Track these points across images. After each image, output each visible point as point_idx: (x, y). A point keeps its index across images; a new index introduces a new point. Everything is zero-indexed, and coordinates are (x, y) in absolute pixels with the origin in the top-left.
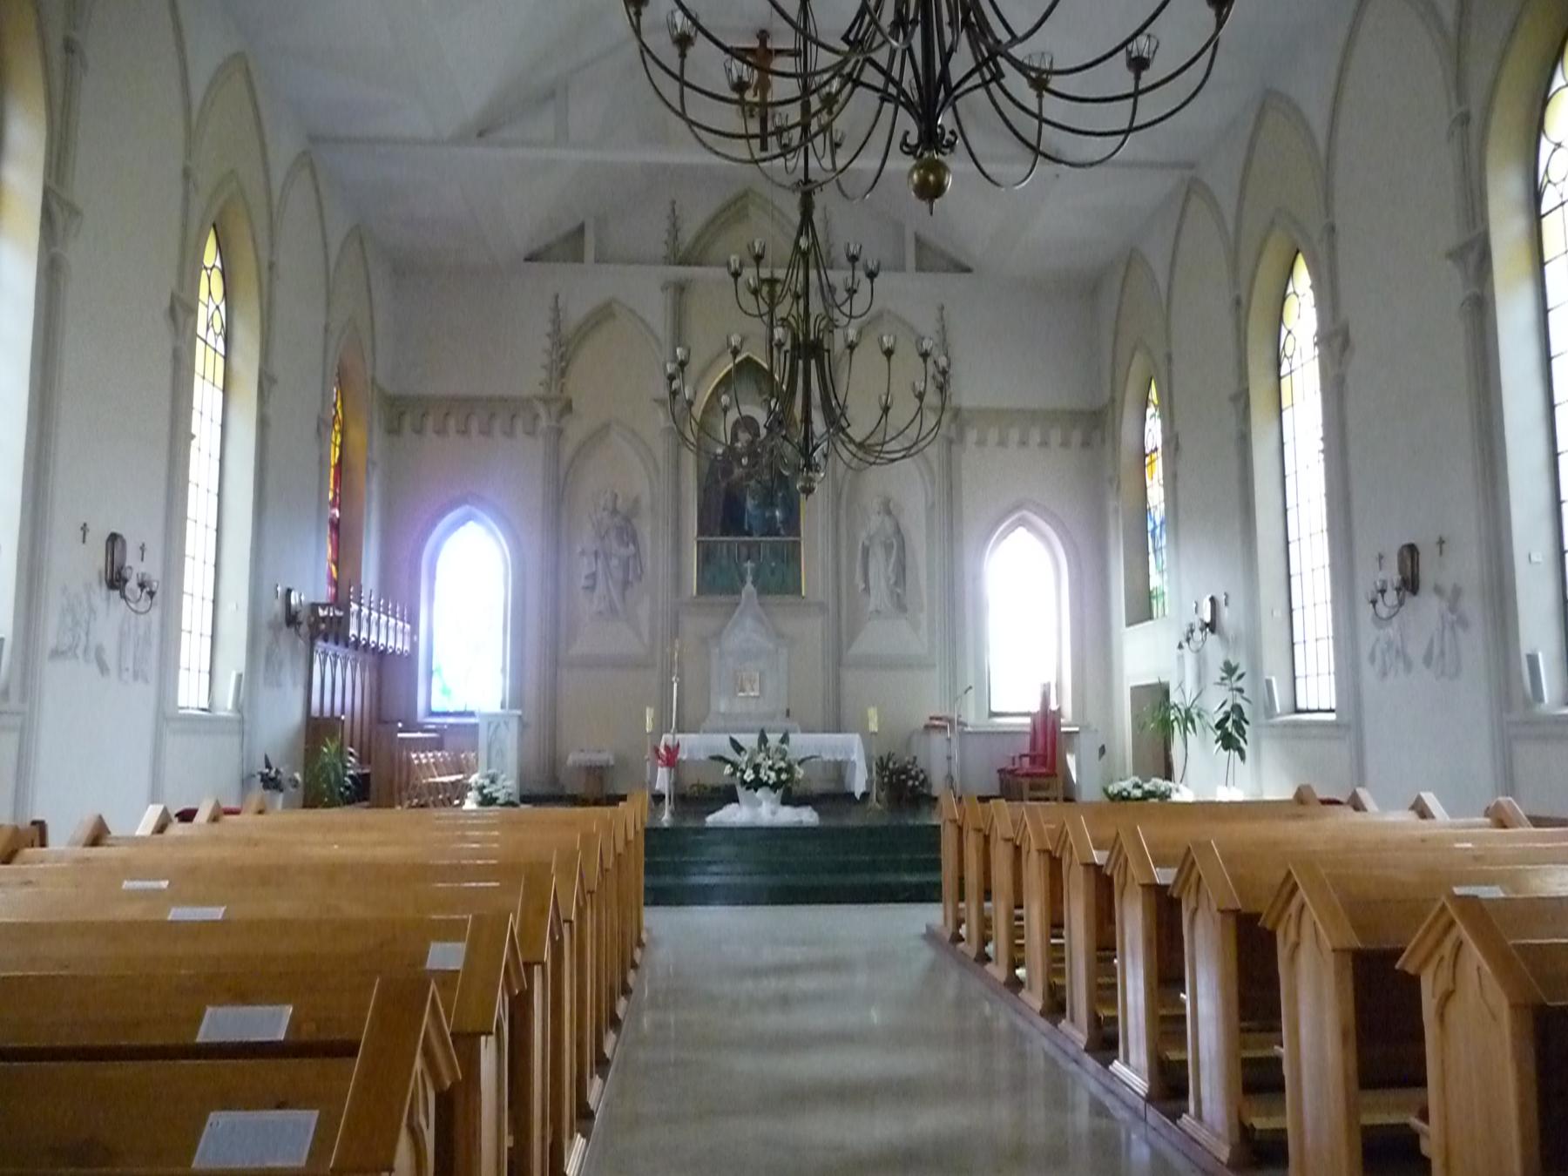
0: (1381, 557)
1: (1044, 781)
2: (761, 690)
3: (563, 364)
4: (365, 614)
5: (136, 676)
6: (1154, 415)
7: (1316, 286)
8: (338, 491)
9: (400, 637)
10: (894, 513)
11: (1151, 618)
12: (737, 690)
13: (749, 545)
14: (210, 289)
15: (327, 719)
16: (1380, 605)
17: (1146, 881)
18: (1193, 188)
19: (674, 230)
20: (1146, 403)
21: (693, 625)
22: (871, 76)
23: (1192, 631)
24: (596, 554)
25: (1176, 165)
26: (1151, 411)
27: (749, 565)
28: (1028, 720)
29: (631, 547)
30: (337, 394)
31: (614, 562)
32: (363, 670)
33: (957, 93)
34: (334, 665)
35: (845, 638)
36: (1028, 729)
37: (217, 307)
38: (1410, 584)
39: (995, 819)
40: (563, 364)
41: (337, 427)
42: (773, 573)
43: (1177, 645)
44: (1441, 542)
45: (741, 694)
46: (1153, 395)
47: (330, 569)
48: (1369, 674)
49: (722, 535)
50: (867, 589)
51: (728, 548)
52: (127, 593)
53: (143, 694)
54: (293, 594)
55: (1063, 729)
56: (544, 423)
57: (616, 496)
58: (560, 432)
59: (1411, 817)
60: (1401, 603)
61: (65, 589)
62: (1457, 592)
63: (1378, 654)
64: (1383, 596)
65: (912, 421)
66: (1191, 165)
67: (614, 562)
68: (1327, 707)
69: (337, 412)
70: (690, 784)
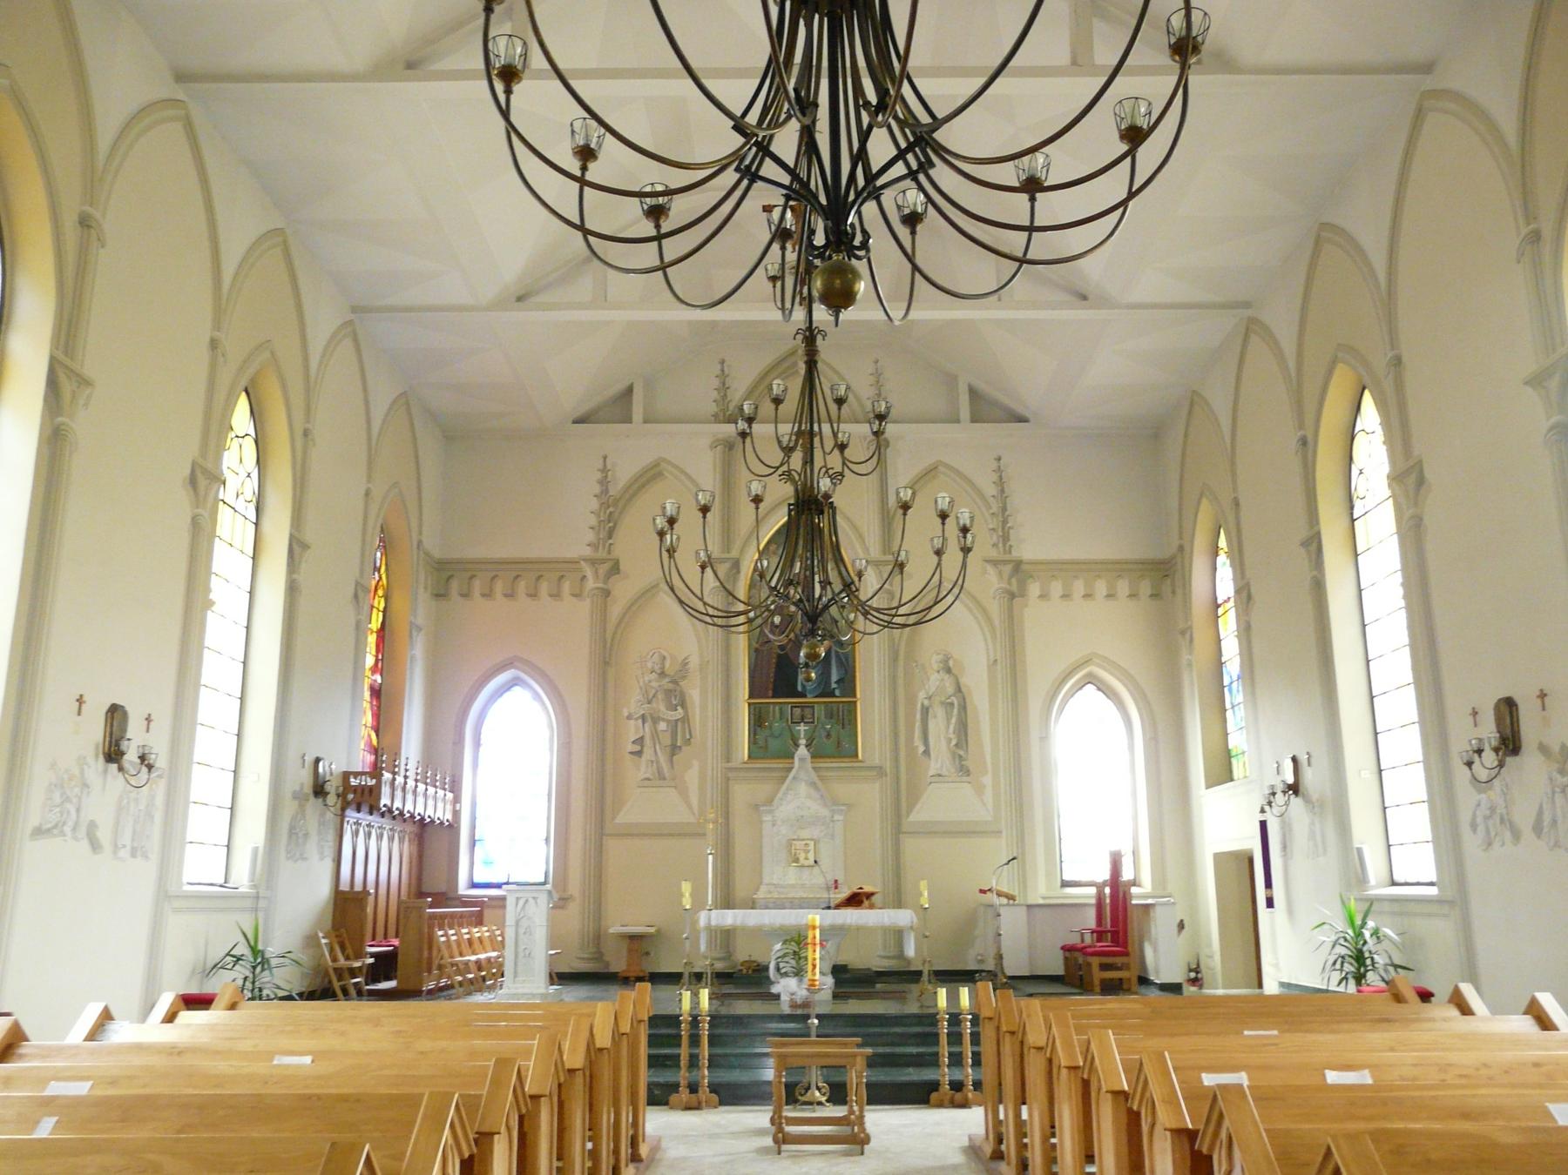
0: (1475, 713)
1: (1118, 960)
3: (611, 525)
4: (400, 783)
5: (133, 855)
6: (1224, 564)
7: (1386, 424)
8: (380, 657)
9: (440, 805)
10: (954, 671)
11: (1232, 780)
13: (802, 707)
14: (238, 460)
15: (358, 893)
16: (1476, 766)
17: (1174, 1126)
18: (1252, 328)
19: (724, 388)
20: (1215, 552)
21: (743, 793)
22: (769, 169)
23: (1274, 794)
24: (643, 718)
26: (1222, 559)
27: (802, 728)
28: (1093, 891)
29: (679, 709)
30: (381, 559)
31: (662, 726)
32: (401, 841)
33: (879, 182)
34: (380, 837)
36: (1093, 901)
37: (249, 476)
38: (1510, 744)
39: (1027, 1025)
40: (611, 525)
41: (380, 592)
42: (828, 736)
43: (1259, 810)
44: (1543, 695)
46: (1222, 542)
47: (369, 736)
48: (1472, 843)
49: (773, 697)
50: (927, 752)
51: (781, 709)
52: (126, 765)
53: (145, 872)
54: (321, 764)
55: (1134, 902)
56: (591, 583)
57: (664, 658)
58: (607, 593)
59: (1526, 1025)
60: (1501, 765)
61: (53, 765)
63: (1479, 820)
64: (1480, 757)
65: (934, 574)
66: (1247, 305)
67: (662, 726)
69: (380, 578)
70: (741, 960)
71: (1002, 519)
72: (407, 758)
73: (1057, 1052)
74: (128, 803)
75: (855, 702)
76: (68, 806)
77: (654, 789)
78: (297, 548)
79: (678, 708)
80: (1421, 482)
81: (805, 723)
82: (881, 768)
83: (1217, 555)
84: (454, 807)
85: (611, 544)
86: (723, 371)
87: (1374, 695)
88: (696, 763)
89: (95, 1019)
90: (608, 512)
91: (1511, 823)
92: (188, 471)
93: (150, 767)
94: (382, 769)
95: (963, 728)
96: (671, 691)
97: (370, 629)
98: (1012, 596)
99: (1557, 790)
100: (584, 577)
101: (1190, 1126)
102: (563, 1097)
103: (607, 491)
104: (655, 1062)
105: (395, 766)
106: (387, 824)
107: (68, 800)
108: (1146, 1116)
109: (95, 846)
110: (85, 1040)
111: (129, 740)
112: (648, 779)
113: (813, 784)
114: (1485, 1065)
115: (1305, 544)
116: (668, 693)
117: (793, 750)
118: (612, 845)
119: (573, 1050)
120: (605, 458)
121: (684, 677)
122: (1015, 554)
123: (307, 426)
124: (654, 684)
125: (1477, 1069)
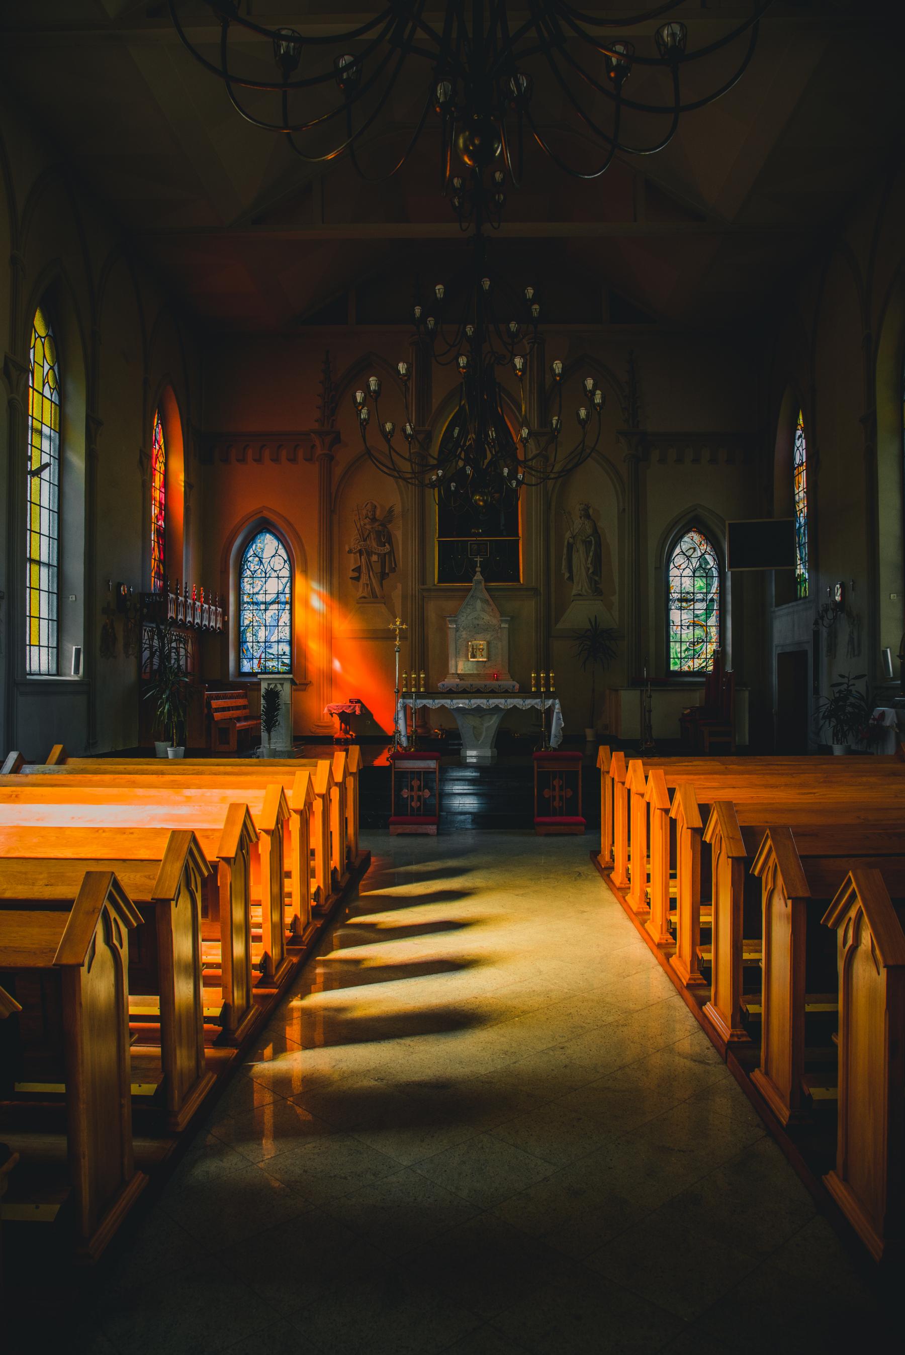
27: (478, 559)
31: (374, 558)
45: (471, 660)
50: (571, 578)
67: (374, 558)
84: (223, 618)
95: (598, 561)
112: (364, 597)
113: (485, 601)
121: (390, 522)
124: (368, 527)
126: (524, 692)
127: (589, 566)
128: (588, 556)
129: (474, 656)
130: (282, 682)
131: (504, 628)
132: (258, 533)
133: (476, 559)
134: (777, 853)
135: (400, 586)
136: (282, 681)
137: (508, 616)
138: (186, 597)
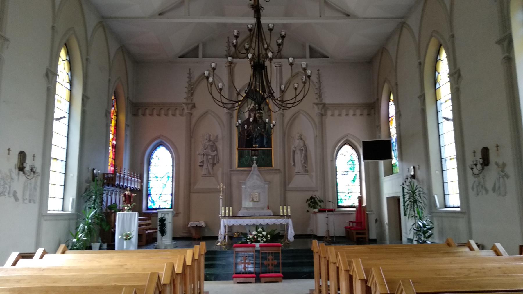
0: (474, 152)
2: (259, 200)
3: (192, 92)
5: (30, 202)
6: (392, 104)
9: (136, 183)
11: (393, 174)
12: (251, 200)
13: (255, 150)
16: (475, 170)
23: (407, 178)
25: (398, 18)
26: (391, 102)
27: (255, 157)
31: (210, 157)
34: (116, 194)
35: (287, 182)
40: (192, 92)
44: (497, 146)
45: (252, 201)
46: (392, 97)
48: (472, 193)
49: (245, 148)
50: (294, 165)
52: (26, 172)
53: (34, 208)
56: (186, 111)
57: (210, 135)
58: (191, 114)
60: (483, 169)
62: (504, 165)
63: (475, 187)
67: (210, 157)
68: (457, 206)
71: (319, 90)
72: (125, 169)
73: (340, 263)
74: (27, 184)
75: (271, 149)
76: (6, 186)
77: (208, 178)
78: (85, 99)
79: (215, 151)
80: (459, 76)
81: (256, 156)
82: (280, 170)
83: (389, 101)
84: (141, 184)
85: (192, 98)
86: (228, 41)
87: (441, 146)
88: (221, 169)
89: (15, 259)
90: (191, 88)
91: (485, 188)
92: (45, 72)
93: (34, 172)
94: (116, 172)
95: (306, 158)
96: (212, 146)
97: (111, 126)
98: (322, 115)
99: (501, 177)
100: (183, 109)
101: (389, 292)
102: (175, 283)
103: (191, 81)
104: (207, 266)
105: (121, 171)
106: (118, 190)
107: (6, 184)
108: (373, 288)
109: (16, 199)
110: (11, 266)
111: (27, 163)
112: (205, 174)
113: (258, 176)
114: (483, 268)
115: (420, 97)
116: (212, 146)
117: (252, 164)
118: (194, 196)
119: (178, 267)
120: (190, 69)
121: (217, 142)
122: (324, 101)
123: (88, 57)
124: (207, 144)
125: (480, 270)
126: (276, 215)
127: (302, 160)
128: (301, 157)
129: (253, 200)
130: (168, 213)
131: (266, 187)
132: (158, 146)
133: (253, 157)
134: (406, 292)
135: (221, 169)
136: (168, 213)
137: (268, 182)
138: (124, 175)
